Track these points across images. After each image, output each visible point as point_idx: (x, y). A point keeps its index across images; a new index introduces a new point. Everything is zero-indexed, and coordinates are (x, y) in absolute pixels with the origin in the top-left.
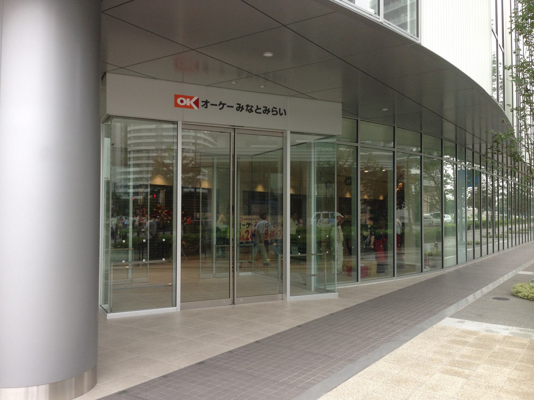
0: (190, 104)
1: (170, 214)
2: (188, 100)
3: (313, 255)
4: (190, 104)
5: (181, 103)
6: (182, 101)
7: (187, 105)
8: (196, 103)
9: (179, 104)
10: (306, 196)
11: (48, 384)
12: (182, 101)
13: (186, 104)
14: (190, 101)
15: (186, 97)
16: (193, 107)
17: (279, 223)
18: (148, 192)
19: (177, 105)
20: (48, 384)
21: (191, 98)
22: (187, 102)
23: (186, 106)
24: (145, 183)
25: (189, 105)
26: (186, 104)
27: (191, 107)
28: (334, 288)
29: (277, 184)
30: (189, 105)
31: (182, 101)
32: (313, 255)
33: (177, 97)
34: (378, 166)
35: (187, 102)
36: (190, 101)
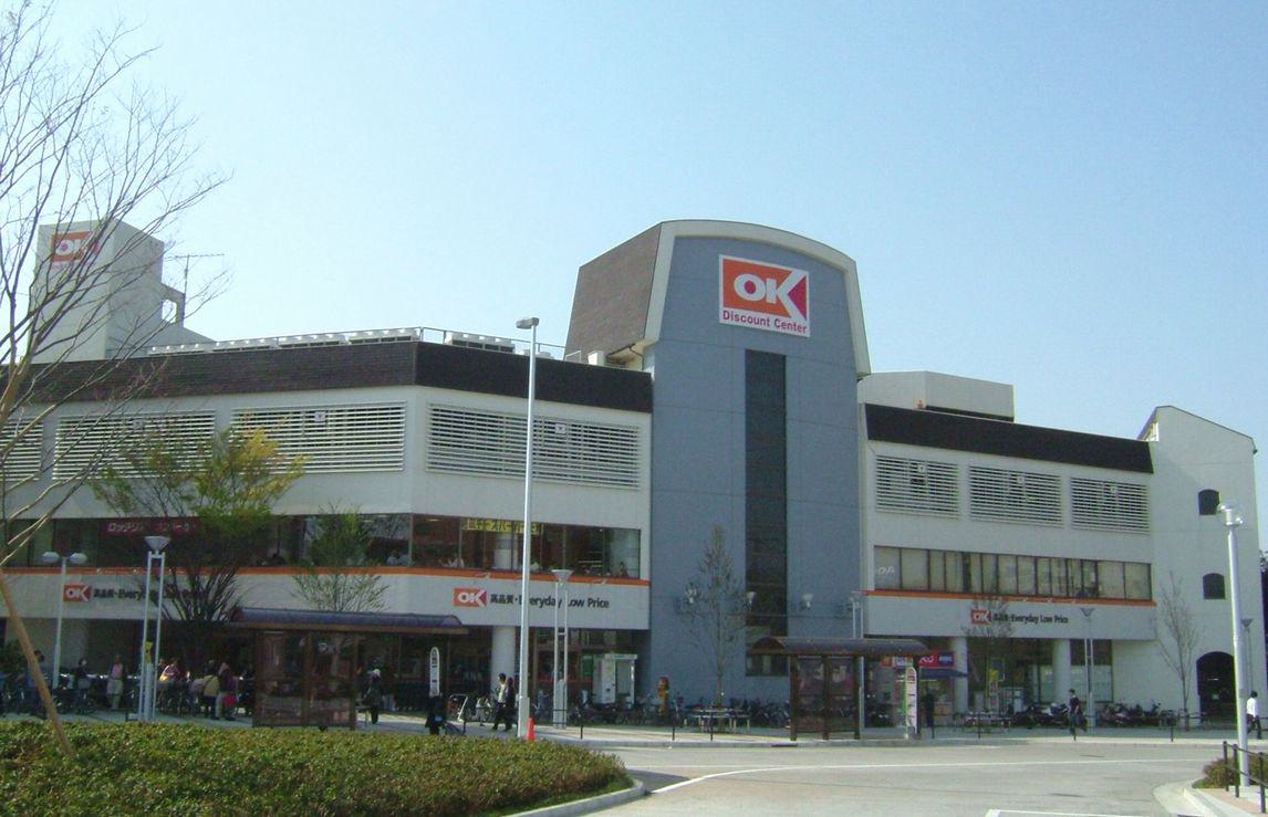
1: (1210, 775)
2: (771, 282)
3: (961, 675)
6: (750, 288)
8: (483, 598)
9: (740, 294)
10: (749, 623)
13: (765, 298)
14: (778, 287)
15: (469, 591)
16: (785, 310)
17: (1136, 583)
21: (780, 277)
22: (471, 598)
23: (469, 604)
26: (765, 298)
27: (475, 605)
29: (859, 560)
31: (464, 597)
32: (961, 675)
33: (458, 591)
35: (471, 598)
36: (778, 287)
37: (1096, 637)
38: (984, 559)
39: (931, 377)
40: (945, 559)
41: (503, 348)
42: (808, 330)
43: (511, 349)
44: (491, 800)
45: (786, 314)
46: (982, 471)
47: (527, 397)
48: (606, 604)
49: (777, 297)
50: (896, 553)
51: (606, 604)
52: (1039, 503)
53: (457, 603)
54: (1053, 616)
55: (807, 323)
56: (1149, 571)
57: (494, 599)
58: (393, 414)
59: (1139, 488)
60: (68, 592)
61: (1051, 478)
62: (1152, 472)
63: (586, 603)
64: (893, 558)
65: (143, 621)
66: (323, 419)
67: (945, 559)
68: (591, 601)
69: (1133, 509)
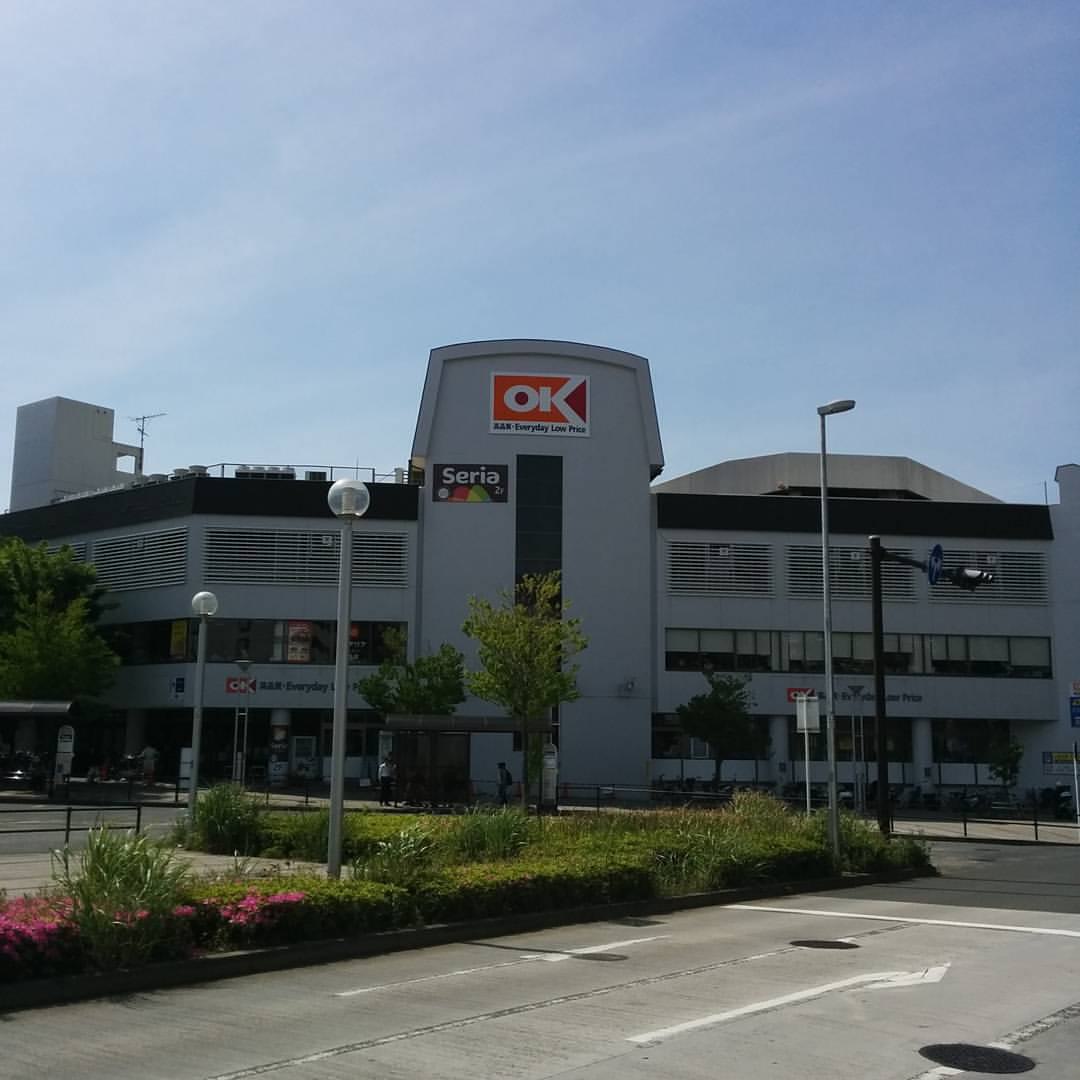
0: (553, 406)
2: (546, 391)
4: (553, 406)
5: (521, 393)
7: (549, 389)
9: (514, 409)
11: (511, 734)
12: (522, 398)
13: (538, 407)
14: (552, 395)
15: (537, 383)
18: (208, 660)
19: (502, 412)
20: (511, 734)
21: (556, 385)
23: (535, 414)
24: (345, 670)
25: (549, 410)
26: (538, 407)
27: (555, 415)
28: (202, 627)
30: (549, 410)
31: (522, 398)
33: (502, 384)
34: (760, 693)
35: (541, 399)
36: (552, 395)
37: (866, 715)
38: (1012, 643)
39: (902, 464)
40: (923, 641)
41: (284, 475)
42: (587, 431)
43: (292, 476)
44: (165, 842)
45: (565, 420)
46: (685, 546)
47: (821, 531)
48: (919, 699)
49: (552, 404)
50: (801, 634)
51: (919, 699)
52: (752, 573)
53: (229, 690)
54: (901, 694)
55: (587, 426)
56: (671, 629)
57: (263, 686)
58: (182, 535)
59: (1037, 556)
60: (231, 686)
61: (764, 548)
62: (1051, 537)
63: (901, 698)
64: (845, 641)
65: (191, 710)
66: (142, 545)
67: (923, 641)
68: (905, 697)
69: (1027, 581)
